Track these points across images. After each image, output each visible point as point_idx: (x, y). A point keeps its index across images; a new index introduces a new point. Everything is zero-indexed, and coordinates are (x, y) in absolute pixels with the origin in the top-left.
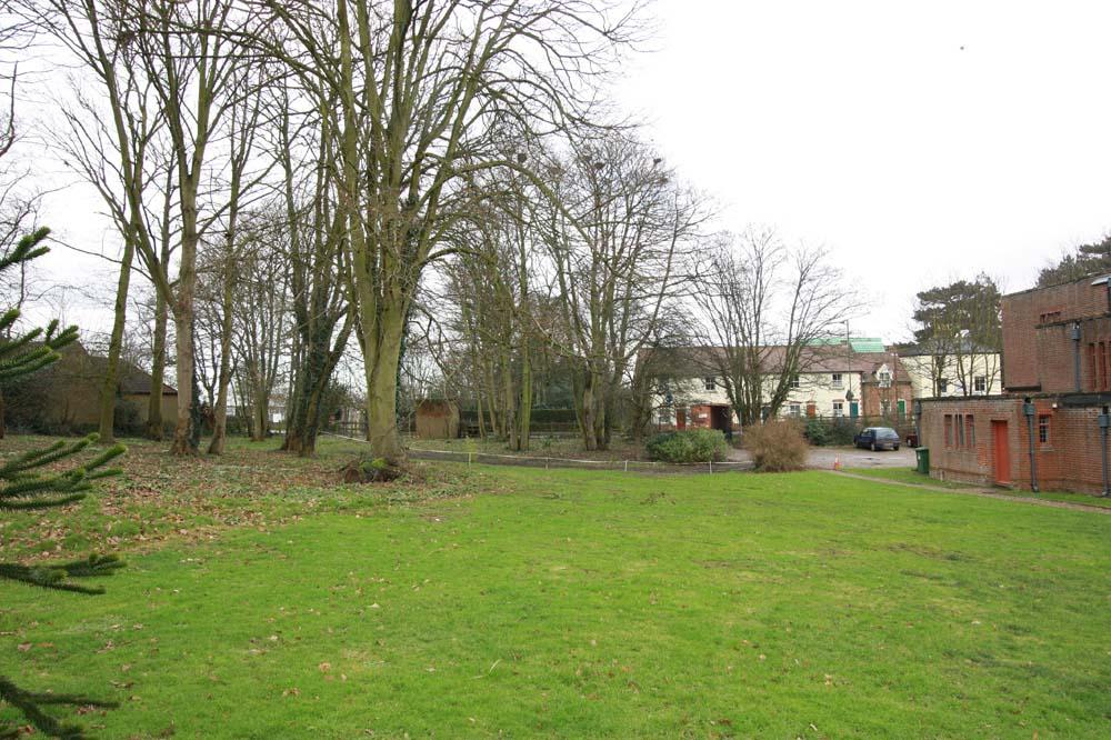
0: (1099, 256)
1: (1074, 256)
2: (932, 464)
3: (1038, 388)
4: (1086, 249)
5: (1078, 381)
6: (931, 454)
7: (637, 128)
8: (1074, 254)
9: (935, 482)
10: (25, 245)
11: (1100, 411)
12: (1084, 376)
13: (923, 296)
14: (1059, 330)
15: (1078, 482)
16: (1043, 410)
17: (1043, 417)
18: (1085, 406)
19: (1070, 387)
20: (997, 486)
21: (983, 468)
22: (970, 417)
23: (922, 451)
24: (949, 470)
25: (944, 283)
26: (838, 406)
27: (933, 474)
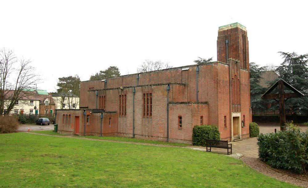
0: (104, 74)
1: (99, 73)
2: (58, 129)
3: (87, 108)
4: (101, 72)
7: (132, 94)
11: (101, 114)
14: (93, 92)
15: (95, 133)
16: (88, 114)
17: (88, 116)
18: (98, 113)
19: (95, 107)
20: (75, 135)
21: (72, 130)
22: (70, 115)
23: (56, 125)
24: (63, 131)
25: (66, 76)
26: (31, 111)
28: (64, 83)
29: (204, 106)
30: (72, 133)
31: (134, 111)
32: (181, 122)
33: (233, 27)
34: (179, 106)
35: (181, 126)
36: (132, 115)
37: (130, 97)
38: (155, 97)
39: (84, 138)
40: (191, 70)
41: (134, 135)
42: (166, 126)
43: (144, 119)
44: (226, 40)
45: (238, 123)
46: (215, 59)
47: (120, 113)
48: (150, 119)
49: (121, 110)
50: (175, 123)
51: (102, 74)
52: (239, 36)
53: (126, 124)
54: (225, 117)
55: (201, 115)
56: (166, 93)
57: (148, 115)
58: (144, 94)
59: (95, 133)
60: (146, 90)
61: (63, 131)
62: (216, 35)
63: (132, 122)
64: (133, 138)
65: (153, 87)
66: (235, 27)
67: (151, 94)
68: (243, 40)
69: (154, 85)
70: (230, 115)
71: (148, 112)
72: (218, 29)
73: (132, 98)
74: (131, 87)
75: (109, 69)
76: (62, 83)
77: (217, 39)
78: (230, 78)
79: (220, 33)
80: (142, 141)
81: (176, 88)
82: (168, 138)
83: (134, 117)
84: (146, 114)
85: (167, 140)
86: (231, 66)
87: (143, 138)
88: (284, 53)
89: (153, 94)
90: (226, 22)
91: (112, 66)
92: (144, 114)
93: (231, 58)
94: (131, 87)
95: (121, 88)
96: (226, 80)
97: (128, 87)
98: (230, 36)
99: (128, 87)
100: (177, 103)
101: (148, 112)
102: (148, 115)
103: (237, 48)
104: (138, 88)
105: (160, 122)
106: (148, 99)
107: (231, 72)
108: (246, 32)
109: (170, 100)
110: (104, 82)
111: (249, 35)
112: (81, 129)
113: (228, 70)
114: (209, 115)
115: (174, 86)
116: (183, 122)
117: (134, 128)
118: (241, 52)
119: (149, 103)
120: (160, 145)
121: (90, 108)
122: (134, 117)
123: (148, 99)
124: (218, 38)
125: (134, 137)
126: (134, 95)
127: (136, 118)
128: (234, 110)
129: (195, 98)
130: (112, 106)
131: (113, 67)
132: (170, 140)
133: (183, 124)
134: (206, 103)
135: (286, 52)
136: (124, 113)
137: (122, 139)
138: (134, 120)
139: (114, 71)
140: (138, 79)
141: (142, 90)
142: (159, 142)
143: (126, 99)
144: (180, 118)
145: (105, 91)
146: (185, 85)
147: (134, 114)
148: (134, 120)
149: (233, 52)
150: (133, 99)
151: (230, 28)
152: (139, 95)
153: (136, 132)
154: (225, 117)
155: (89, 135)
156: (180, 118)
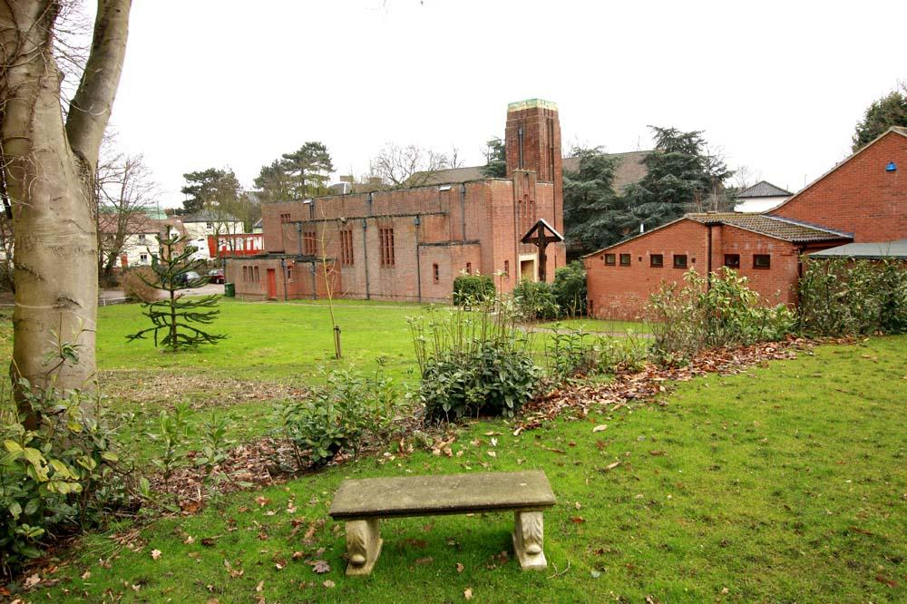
0: (292, 161)
1: (279, 160)
2: (236, 291)
3: (283, 252)
4: (285, 156)
5: (301, 249)
6: (236, 286)
7: (362, 230)
8: (280, 159)
9: (239, 300)
10: (836, 381)
11: (311, 264)
12: (303, 247)
13: (188, 177)
14: (292, 225)
15: (304, 295)
16: (289, 264)
17: (289, 267)
18: (305, 262)
19: (297, 252)
20: (271, 299)
21: (264, 291)
22: (256, 267)
23: (229, 286)
24: (246, 294)
25: (202, 169)
26: (143, 257)
27: (236, 296)
28: (198, 187)
29: (472, 247)
30: (263, 297)
31: (366, 258)
32: (437, 273)
33: (530, 107)
34: (433, 249)
35: (437, 279)
36: (363, 263)
37: (358, 234)
38: (398, 234)
39: (288, 303)
40: (453, 190)
41: (369, 295)
42: (417, 278)
43: (383, 270)
44: (519, 128)
45: (532, 270)
46: (36, 574)
47: (348, 261)
48: (393, 270)
49: (345, 256)
50: (428, 274)
51: (288, 160)
52: (540, 123)
53: (355, 279)
54: (506, 262)
55: (468, 261)
56: (415, 229)
57: (388, 262)
58: (381, 230)
59: (304, 295)
60: (384, 223)
61: (246, 294)
62: (505, 119)
63: (364, 274)
64: (368, 299)
65: (394, 219)
66: (534, 106)
67: (392, 230)
68: (548, 128)
69: (395, 216)
70: (516, 259)
71: (388, 259)
72: (506, 108)
73: (362, 236)
74: (359, 218)
75: (304, 149)
76: (192, 187)
77: (505, 126)
78: (514, 202)
79: (512, 115)
80: (382, 303)
81: (429, 221)
82: (420, 296)
83: (366, 267)
84: (386, 262)
85: (419, 300)
86: (516, 182)
87: (384, 298)
88: (657, 129)
89: (394, 231)
90: (520, 97)
91: (311, 141)
92: (383, 262)
93: (517, 169)
94: (359, 218)
95: (343, 219)
96: (507, 204)
97: (354, 219)
98: (526, 122)
99: (354, 219)
100: (431, 244)
101: (388, 259)
102: (388, 262)
103: (536, 146)
104: (370, 219)
105: (408, 274)
106: (387, 236)
107: (516, 192)
108: (557, 112)
109: (421, 240)
110: (308, 207)
111: (562, 118)
112: (280, 290)
113: (512, 189)
114: (481, 260)
115: (426, 217)
116: (439, 273)
117: (368, 285)
118: (544, 156)
119: (390, 243)
120: (408, 307)
121: (289, 251)
122: (366, 267)
123: (387, 236)
124: (508, 124)
125: (368, 299)
126: (365, 231)
127: (371, 268)
128: (523, 251)
129: (461, 234)
130: (328, 248)
131: (315, 146)
132: (423, 300)
133: (440, 275)
134: (476, 242)
135: (660, 127)
136: (350, 261)
137: (350, 301)
138: (367, 271)
139: (316, 154)
140: (371, 201)
141: (378, 224)
142: (411, 303)
143: (351, 238)
144: (436, 266)
145: (313, 224)
146: (444, 214)
147: (366, 261)
148: (367, 271)
149: (530, 149)
150: (362, 237)
151: (525, 108)
152: (373, 232)
153: (371, 291)
154: (506, 262)
155: (294, 299)
156: (436, 266)
